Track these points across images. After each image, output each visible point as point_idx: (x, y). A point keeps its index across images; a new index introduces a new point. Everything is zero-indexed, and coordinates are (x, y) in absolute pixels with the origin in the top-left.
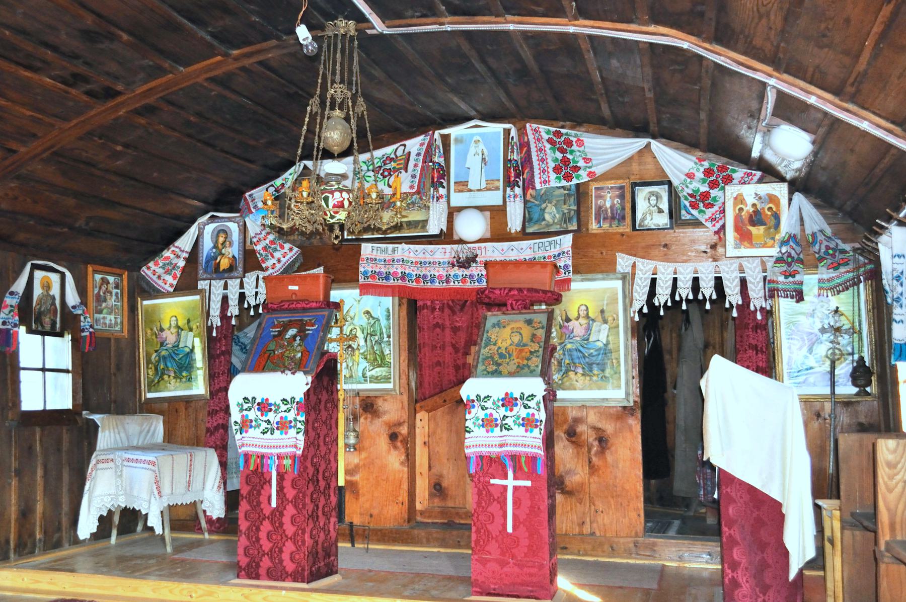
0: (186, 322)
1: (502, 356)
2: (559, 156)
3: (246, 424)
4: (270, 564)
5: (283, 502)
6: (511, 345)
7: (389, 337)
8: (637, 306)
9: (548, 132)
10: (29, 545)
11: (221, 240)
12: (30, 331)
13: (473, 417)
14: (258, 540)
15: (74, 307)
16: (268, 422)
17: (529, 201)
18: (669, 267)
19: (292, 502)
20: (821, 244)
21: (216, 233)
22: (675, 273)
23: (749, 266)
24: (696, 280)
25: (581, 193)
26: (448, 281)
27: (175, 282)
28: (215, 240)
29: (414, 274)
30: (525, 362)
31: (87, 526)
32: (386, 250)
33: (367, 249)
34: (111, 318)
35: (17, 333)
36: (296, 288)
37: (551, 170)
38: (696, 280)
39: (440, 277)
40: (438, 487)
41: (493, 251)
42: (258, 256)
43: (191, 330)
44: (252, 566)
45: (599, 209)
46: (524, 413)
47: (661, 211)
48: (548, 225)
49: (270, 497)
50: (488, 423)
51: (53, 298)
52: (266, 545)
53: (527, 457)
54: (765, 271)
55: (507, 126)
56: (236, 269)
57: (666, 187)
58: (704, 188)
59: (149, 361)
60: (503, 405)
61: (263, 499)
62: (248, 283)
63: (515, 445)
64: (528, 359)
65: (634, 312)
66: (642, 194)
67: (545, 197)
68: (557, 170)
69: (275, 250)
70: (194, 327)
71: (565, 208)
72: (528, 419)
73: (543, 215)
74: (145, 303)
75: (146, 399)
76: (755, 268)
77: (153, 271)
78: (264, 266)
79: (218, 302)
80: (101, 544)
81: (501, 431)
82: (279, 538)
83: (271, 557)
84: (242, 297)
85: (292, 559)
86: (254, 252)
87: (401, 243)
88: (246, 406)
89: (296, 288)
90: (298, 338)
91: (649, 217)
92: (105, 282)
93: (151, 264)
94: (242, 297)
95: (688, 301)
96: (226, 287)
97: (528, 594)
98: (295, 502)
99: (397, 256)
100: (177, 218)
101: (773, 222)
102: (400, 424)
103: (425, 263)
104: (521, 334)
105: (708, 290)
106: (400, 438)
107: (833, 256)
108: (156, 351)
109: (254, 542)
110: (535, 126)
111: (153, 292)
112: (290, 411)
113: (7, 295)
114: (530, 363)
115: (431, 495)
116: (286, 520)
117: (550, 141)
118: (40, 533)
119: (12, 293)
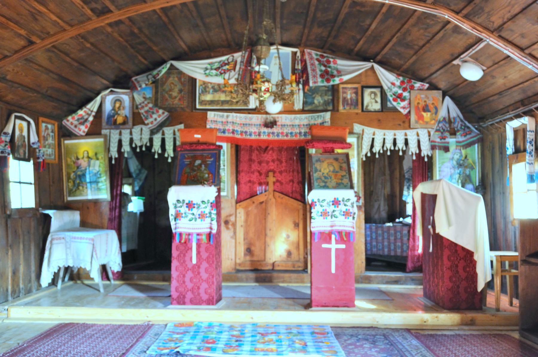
0: (94, 154)
1: (325, 177)
2: (323, 68)
3: (178, 216)
4: (192, 296)
5: (200, 260)
6: (329, 172)
7: (224, 166)
8: (364, 152)
9: (317, 55)
10: (17, 291)
11: (117, 105)
12: (15, 158)
13: (316, 212)
14: (184, 282)
15: (33, 144)
16: (193, 214)
17: (306, 93)
18: (401, 132)
19: (205, 260)
20: (458, 123)
21: (113, 101)
22: (384, 135)
23: (421, 133)
24: (395, 140)
25: (334, 90)
26: (259, 135)
27: (86, 130)
28: (113, 105)
29: (239, 130)
30: (340, 181)
31: (46, 278)
32: (223, 116)
33: (211, 115)
34: (50, 151)
35: (9, 158)
36: (199, 136)
37: (318, 76)
38: (395, 140)
39: (255, 133)
40: (248, 250)
41: (286, 120)
42: (142, 116)
43: (98, 159)
44: (180, 298)
45: (345, 99)
46: (344, 208)
47: (376, 102)
48: (317, 106)
49: (191, 258)
50: (324, 214)
51: (24, 137)
52: (190, 285)
53: (346, 233)
54: (429, 135)
55: (295, 50)
56: (128, 123)
57: (364, 89)
58: (400, 91)
59: (69, 178)
60: (333, 204)
61: (187, 258)
62: (135, 132)
63: (340, 226)
64: (342, 180)
65: (363, 155)
66: (367, 92)
67: (315, 91)
68: (322, 76)
69: (153, 113)
70: (100, 157)
71: (326, 98)
72: (347, 212)
73: (313, 101)
74: (67, 142)
75: (67, 201)
76: (425, 134)
77: (70, 121)
78: (146, 122)
79: (116, 142)
80: (53, 289)
81: (332, 218)
82: (198, 280)
83: (193, 292)
84: (131, 141)
85: (206, 293)
86: (139, 114)
87: (232, 112)
88: (179, 205)
89: (199, 136)
90: (203, 166)
91: (370, 105)
92: (47, 128)
93: (70, 118)
94: (131, 141)
95: (390, 150)
96: (120, 134)
97: (345, 305)
98: (208, 260)
99: (230, 119)
100: (91, 90)
101: (434, 111)
102: (230, 215)
103: (246, 124)
104: (333, 166)
105: (400, 145)
106: (230, 223)
107: (464, 130)
108: (74, 172)
109: (182, 284)
110: (309, 51)
111: (69, 135)
112: (206, 207)
113: (2, 134)
114: (343, 182)
115: (245, 255)
116: (202, 270)
117: (318, 60)
118: (22, 284)
119: (5, 133)
